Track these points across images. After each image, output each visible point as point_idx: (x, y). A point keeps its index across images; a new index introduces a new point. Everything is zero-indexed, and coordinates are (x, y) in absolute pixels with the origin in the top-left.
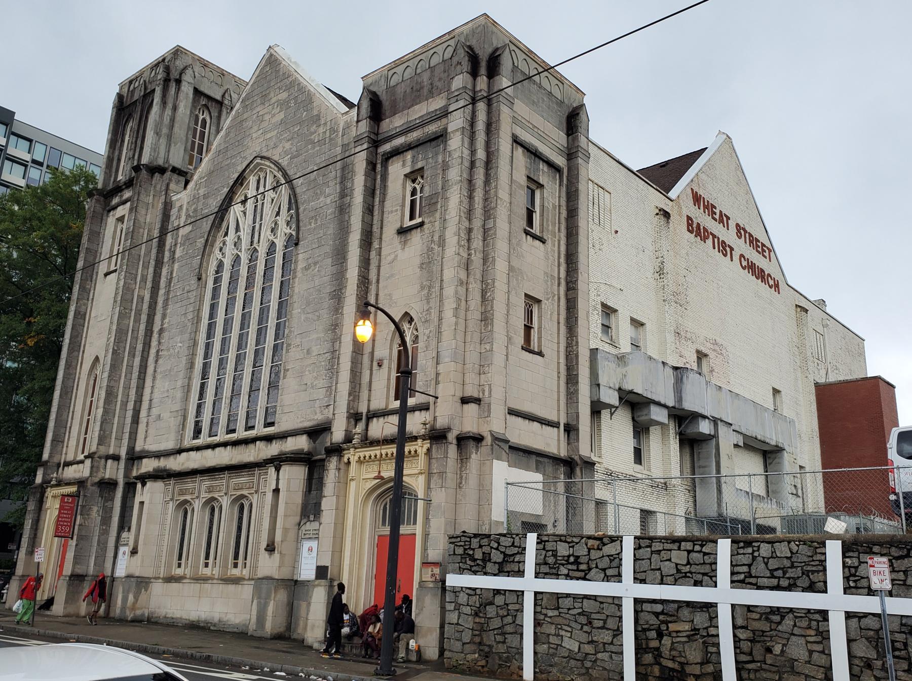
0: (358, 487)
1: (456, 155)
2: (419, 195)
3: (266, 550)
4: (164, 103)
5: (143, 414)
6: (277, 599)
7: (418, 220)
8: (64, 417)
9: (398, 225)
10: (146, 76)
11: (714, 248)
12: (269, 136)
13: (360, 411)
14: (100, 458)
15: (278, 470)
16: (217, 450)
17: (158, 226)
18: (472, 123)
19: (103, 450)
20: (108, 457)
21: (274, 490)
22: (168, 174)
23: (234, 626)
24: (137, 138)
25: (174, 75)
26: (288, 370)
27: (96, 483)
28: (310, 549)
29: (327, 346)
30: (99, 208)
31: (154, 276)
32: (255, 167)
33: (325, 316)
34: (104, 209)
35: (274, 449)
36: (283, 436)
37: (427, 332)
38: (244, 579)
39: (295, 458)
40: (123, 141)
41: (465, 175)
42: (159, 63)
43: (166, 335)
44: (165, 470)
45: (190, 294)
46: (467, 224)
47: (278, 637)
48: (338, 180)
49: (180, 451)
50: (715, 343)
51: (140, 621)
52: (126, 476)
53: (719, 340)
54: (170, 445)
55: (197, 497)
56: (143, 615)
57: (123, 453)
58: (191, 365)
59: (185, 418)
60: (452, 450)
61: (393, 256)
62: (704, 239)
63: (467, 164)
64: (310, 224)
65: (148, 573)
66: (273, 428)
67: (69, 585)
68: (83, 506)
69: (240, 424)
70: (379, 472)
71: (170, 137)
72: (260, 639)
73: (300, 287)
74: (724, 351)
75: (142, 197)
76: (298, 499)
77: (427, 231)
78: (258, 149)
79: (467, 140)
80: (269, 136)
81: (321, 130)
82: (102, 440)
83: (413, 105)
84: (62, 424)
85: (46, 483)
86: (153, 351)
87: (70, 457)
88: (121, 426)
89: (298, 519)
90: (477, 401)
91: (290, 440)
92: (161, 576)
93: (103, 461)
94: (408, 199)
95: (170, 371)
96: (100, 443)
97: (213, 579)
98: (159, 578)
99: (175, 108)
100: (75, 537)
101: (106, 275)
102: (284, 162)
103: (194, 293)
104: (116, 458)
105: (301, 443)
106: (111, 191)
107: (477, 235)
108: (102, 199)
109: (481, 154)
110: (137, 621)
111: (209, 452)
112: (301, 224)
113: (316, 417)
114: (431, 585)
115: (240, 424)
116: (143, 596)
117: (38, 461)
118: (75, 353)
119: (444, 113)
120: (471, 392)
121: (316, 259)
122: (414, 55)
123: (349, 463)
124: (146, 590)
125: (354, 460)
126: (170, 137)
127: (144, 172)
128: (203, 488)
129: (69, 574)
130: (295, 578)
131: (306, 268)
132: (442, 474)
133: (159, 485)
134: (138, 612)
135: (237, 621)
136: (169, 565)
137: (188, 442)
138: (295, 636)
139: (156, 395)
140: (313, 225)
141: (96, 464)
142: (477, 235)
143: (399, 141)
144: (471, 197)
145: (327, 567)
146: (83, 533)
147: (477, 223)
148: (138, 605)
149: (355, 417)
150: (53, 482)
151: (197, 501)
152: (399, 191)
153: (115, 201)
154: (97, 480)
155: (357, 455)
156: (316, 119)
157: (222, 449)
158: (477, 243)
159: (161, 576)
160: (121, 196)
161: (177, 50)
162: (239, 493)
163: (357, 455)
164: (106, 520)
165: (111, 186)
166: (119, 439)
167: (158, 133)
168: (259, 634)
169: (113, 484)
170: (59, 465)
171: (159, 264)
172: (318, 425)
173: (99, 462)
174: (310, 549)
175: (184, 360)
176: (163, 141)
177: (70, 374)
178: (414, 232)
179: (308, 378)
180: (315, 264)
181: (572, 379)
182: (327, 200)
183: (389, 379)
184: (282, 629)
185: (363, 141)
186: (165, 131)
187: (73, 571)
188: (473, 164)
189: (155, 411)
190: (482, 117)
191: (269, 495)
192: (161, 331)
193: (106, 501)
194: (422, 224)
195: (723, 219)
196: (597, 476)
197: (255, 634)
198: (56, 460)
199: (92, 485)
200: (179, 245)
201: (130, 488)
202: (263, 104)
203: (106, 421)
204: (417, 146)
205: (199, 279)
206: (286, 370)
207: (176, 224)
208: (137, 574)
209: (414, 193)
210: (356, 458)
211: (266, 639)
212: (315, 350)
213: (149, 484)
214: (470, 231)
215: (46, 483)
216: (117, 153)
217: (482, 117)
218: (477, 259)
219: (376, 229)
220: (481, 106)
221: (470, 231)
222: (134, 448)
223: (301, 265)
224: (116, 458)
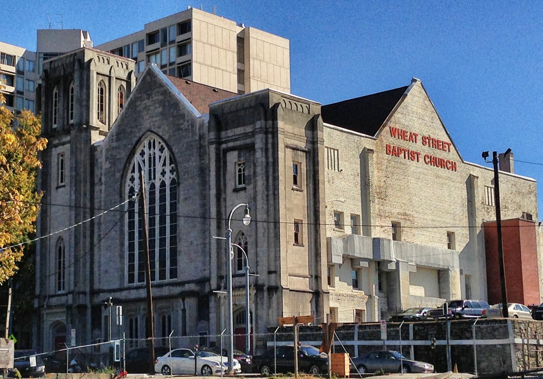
1: (260, 161)
2: (242, 173)
5: (96, 269)
7: (243, 185)
9: (234, 187)
11: (405, 158)
12: (154, 119)
13: (223, 274)
15: (183, 300)
17: (88, 162)
18: (266, 143)
19: (77, 289)
20: (80, 293)
21: (182, 310)
29: (200, 241)
31: (91, 192)
35: (177, 290)
36: (182, 284)
37: (251, 241)
39: (191, 294)
41: (264, 170)
46: (266, 192)
50: (405, 214)
53: (408, 212)
54: (116, 286)
57: (88, 290)
58: (122, 245)
60: (266, 294)
62: (398, 155)
63: (264, 164)
73: (183, 208)
74: (411, 218)
76: (195, 313)
78: (148, 126)
79: (264, 153)
80: (154, 119)
86: (96, 235)
87: (52, 293)
90: (275, 272)
94: (237, 174)
101: (58, 188)
104: (84, 293)
105: (192, 287)
107: (271, 197)
109: (271, 160)
117: (33, 296)
119: (253, 134)
120: (273, 269)
123: (43, 315)
131: (186, 199)
132: (262, 304)
137: (126, 284)
142: (271, 197)
143: (231, 144)
144: (267, 180)
147: (271, 192)
152: (233, 170)
154: (76, 305)
156: (183, 116)
158: (271, 202)
160: (59, 140)
166: (84, 283)
169: (84, 307)
170: (45, 297)
171: (92, 184)
172: (201, 278)
181: (317, 255)
182: (193, 163)
188: (267, 163)
190: (270, 141)
191: (180, 312)
194: (244, 189)
195: (413, 137)
196: (331, 297)
198: (43, 294)
199: (414, 280)
200: (103, 175)
202: (149, 99)
206: (180, 251)
209: (240, 171)
212: (195, 242)
214: (268, 196)
215: (41, 306)
216: (50, 109)
217: (270, 141)
218: (272, 208)
219: (222, 187)
220: (270, 136)
221: (268, 196)
223: (182, 198)
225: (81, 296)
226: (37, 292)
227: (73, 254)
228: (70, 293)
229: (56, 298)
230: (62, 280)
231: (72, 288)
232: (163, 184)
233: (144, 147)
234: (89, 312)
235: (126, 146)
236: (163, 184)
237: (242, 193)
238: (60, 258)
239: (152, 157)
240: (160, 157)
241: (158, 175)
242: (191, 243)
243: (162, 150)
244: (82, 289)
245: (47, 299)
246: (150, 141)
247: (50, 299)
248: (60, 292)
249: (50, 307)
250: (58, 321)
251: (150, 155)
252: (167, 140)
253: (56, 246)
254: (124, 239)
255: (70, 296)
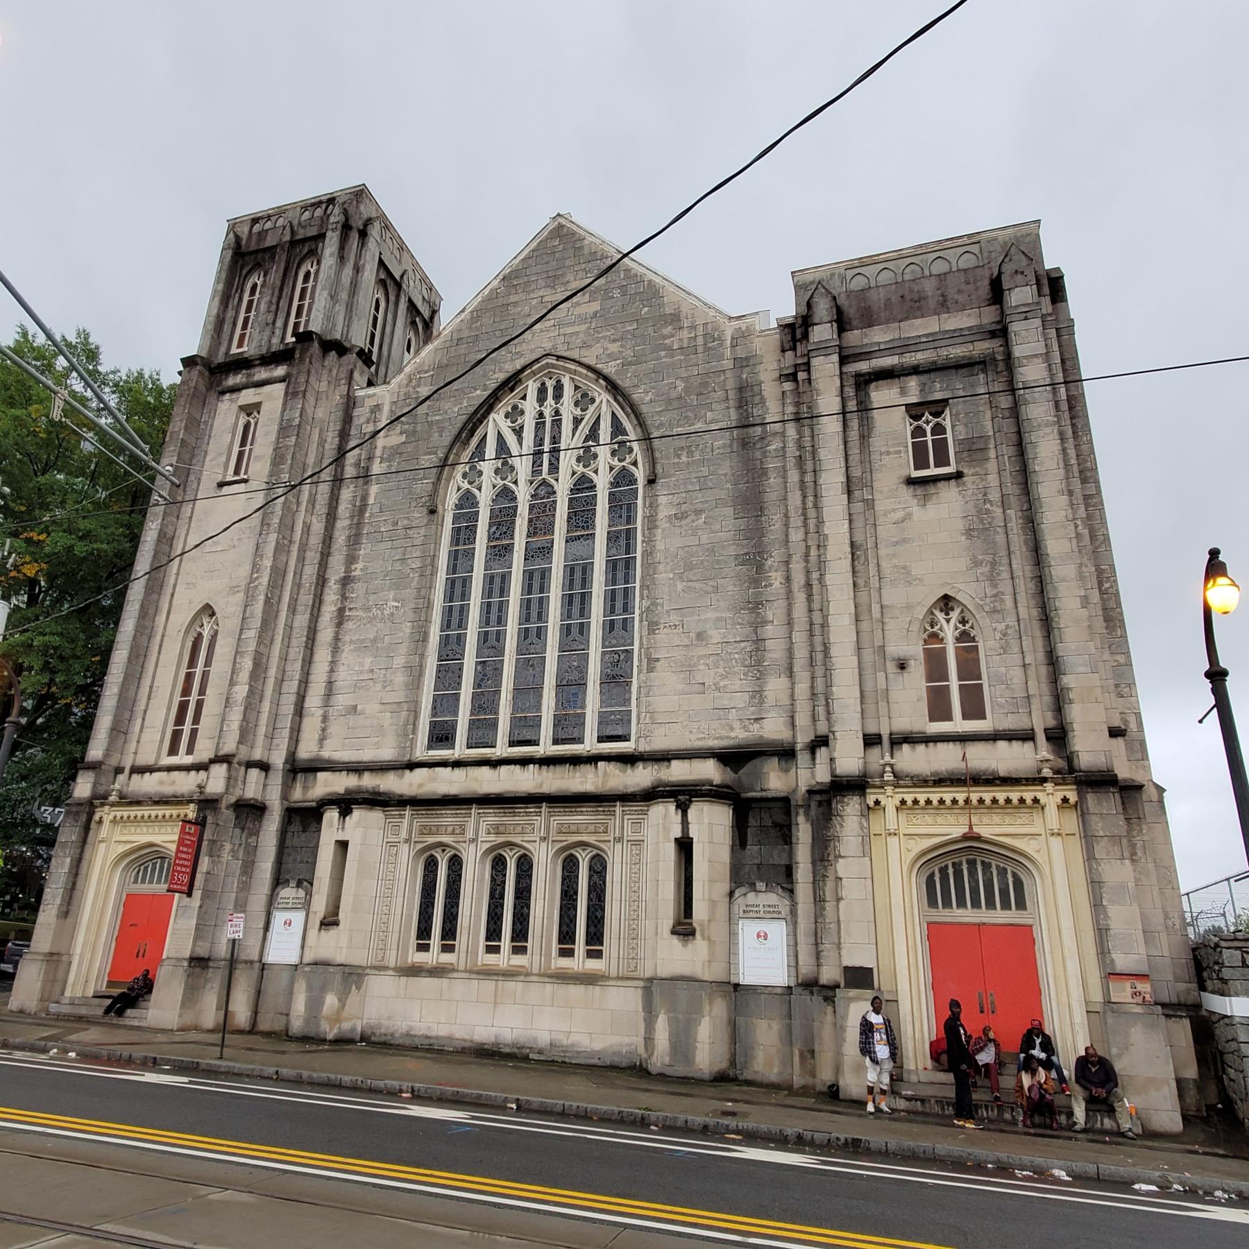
0: (108, 848)
3: (673, 932)
4: (342, 258)
6: (714, 1013)
8: (132, 693)
10: (293, 216)
14: (239, 764)
16: (504, 769)
19: (243, 754)
20: (250, 765)
22: (353, 357)
23: (592, 1054)
24: (280, 298)
25: (357, 223)
26: (658, 660)
27: (232, 805)
28: (288, 923)
30: (202, 388)
32: (541, 370)
33: (731, 588)
34: (209, 389)
35: (641, 777)
38: (608, 978)
40: (241, 299)
42: (321, 202)
43: (358, 590)
44: (377, 793)
45: (410, 532)
47: (721, 1078)
48: (732, 403)
49: (412, 766)
51: (351, 1041)
52: (285, 797)
54: (387, 753)
55: (473, 840)
56: (353, 1029)
57: (278, 759)
59: (416, 714)
61: (901, 514)
64: (679, 456)
65: (359, 958)
66: (493, 750)
67: (189, 976)
68: (212, 842)
69: (546, 730)
70: (971, 827)
71: (350, 308)
72: (685, 1080)
75: (312, 379)
76: (725, 855)
77: (969, 485)
81: (685, 334)
82: (246, 734)
83: (907, 318)
84: (126, 705)
85: (99, 798)
87: (146, 758)
88: (275, 716)
89: (726, 887)
91: (675, 764)
92: (392, 965)
93: (243, 768)
95: (374, 640)
96: (240, 742)
97: (608, 978)
98: (386, 968)
99: (357, 269)
100: (197, 894)
102: (610, 369)
103: (422, 531)
104: (264, 767)
105: (709, 771)
106: (220, 366)
108: (207, 373)
110: (342, 1042)
111: (485, 771)
112: (657, 455)
113: (733, 735)
114: (1138, 1010)
115: (546, 730)
116: (354, 997)
118: (155, 596)
121: (700, 506)
122: (899, 255)
123: (100, 822)
124: (358, 988)
125: (107, 819)
126: (350, 308)
127: (316, 344)
128: (483, 826)
129: (188, 956)
130: (734, 980)
133: (375, 817)
134: (346, 1026)
135: (598, 1046)
136: (402, 947)
138: (747, 1075)
139: (344, 676)
140: (684, 459)
141: (234, 773)
145: (871, 969)
146: (210, 887)
148: (345, 1014)
149: (871, 741)
150: (113, 798)
151: (472, 846)
153: (233, 380)
154: (233, 799)
155: (113, 814)
157: (517, 769)
159: (392, 965)
161: (362, 191)
162: (431, 840)
163: (113, 814)
164: (248, 867)
165: (220, 358)
166: (270, 737)
167: (333, 297)
168: (680, 1070)
172: (740, 747)
173: (238, 771)
174: (288, 923)
175: (407, 628)
176: (340, 310)
177: (144, 627)
178: (941, 484)
179: (706, 675)
180: (698, 512)
183: (163, 733)
184: (723, 1065)
185: (829, 351)
186: (344, 296)
187: (193, 950)
189: (342, 700)
192: (346, 581)
193: (250, 835)
194: (958, 475)
197: (669, 1071)
198: (113, 762)
199: (227, 808)
201: (304, 818)
203: (251, 706)
204: (928, 371)
205: (433, 512)
207: (369, 429)
208: (340, 959)
210: (111, 817)
211: (699, 1082)
212: (715, 636)
213: (357, 814)
215: (99, 798)
222: (294, 753)
224: (264, 767)
225: (254, 773)
226: (95, 752)
227: (252, 646)
228: (217, 760)
229: (156, 775)
230: (187, 728)
231: (229, 747)
232: (583, 485)
233: (524, 398)
234: (272, 825)
235: (31, 646)
236: (583, 485)
237: (948, 492)
238: (192, 663)
239: (548, 420)
240: (577, 421)
241: (567, 462)
242: (700, 636)
243: (584, 400)
244: (257, 755)
245: (121, 778)
246: (543, 384)
247: (134, 776)
248: (174, 760)
249: (127, 800)
250: (152, 845)
251: (541, 415)
252: (614, 377)
253: (187, 631)
254: (428, 621)
255: (219, 771)
